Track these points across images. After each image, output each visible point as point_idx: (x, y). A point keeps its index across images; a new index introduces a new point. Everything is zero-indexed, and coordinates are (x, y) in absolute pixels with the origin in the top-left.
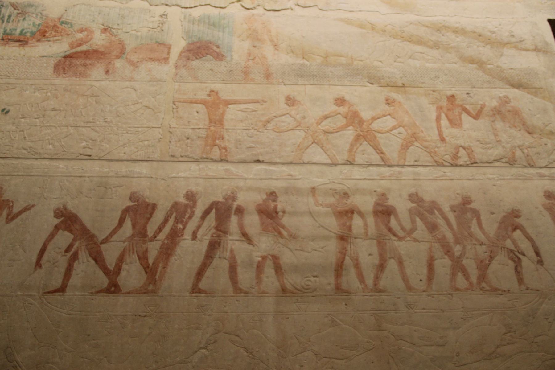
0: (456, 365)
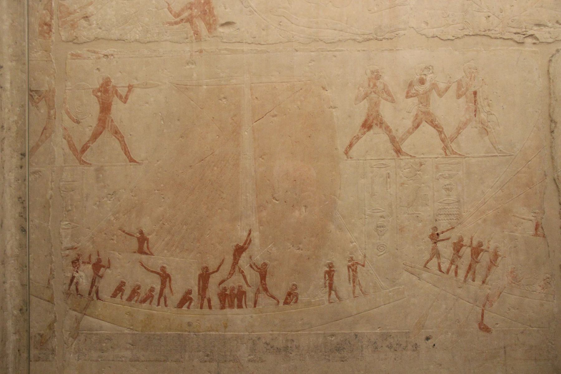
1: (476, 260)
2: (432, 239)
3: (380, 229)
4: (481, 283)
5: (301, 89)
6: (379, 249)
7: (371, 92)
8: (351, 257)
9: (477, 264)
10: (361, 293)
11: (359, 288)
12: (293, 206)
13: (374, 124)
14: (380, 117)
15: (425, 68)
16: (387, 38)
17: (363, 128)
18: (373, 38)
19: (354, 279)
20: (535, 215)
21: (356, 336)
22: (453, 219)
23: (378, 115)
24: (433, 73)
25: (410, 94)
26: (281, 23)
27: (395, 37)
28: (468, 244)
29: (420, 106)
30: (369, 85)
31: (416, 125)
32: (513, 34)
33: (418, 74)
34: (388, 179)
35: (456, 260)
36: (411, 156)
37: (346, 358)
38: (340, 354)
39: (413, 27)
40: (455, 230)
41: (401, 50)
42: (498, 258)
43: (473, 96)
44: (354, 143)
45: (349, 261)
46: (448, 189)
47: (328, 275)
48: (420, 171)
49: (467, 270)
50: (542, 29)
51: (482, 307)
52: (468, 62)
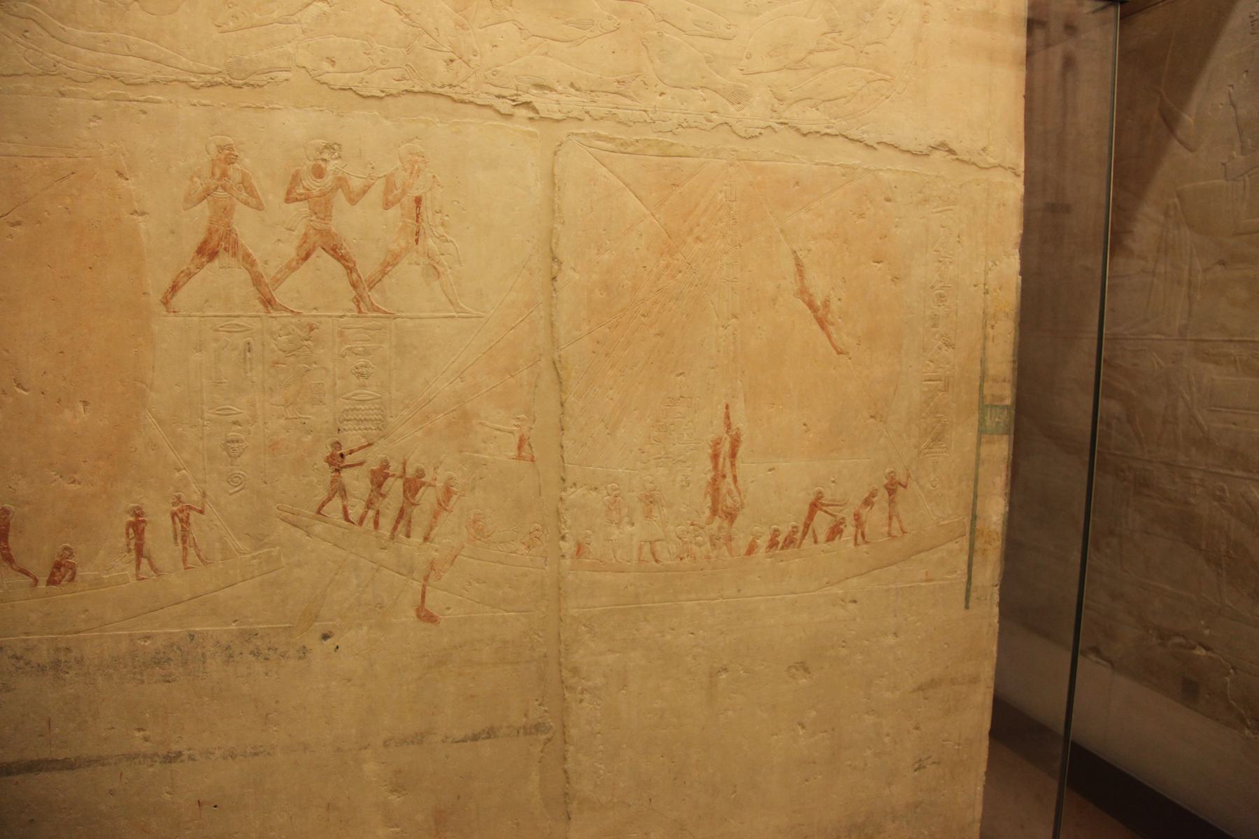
0: (743, 72)
1: (412, 501)
2: (331, 464)
3: (232, 445)
4: (421, 540)
5: (73, 173)
6: (232, 481)
7: (216, 188)
8: (177, 497)
9: (413, 507)
10: (200, 561)
11: (194, 552)
12: (59, 401)
13: (222, 250)
14: (234, 236)
15: (326, 147)
16: (251, 85)
17: (200, 256)
18: (223, 82)
19: (183, 536)
20: (519, 423)
21: (192, 637)
22: (370, 429)
23: (229, 232)
24: (340, 157)
25: (294, 195)
26: (27, 34)
27: (268, 83)
28: (398, 473)
29: (312, 219)
30: (213, 174)
31: (303, 254)
32: (494, 98)
33: (312, 159)
34: (248, 354)
35: (376, 500)
36: (292, 311)
37: (174, 677)
38: (163, 669)
39: (304, 67)
40: (374, 448)
41: (279, 109)
42: (451, 497)
43: (414, 205)
44: (180, 284)
45: (174, 504)
46: (362, 375)
47: (133, 529)
48: (309, 340)
49: (396, 518)
50: (547, 94)
51: (422, 581)
52: (408, 142)
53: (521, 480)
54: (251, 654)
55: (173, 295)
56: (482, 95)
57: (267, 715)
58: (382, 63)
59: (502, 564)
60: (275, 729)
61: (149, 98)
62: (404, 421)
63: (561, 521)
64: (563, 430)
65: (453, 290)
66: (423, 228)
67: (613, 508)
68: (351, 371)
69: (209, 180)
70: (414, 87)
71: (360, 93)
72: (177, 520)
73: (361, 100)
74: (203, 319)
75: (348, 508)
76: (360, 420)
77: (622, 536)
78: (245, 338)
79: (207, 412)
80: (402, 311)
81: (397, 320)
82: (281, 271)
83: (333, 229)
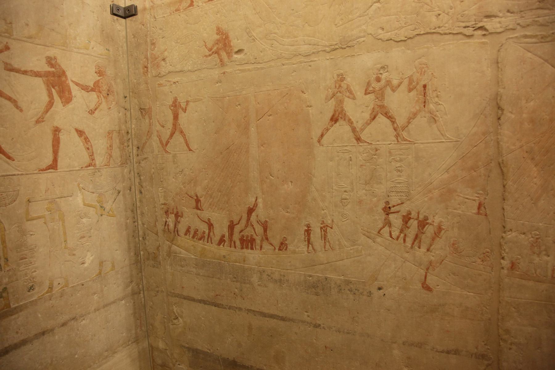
1: (422, 231)
2: (384, 211)
4: (425, 250)
5: (287, 94)
7: (337, 92)
13: (340, 118)
14: (345, 112)
15: (381, 68)
18: (338, 48)
19: (324, 237)
21: (326, 279)
22: (403, 196)
24: (387, 71)
25: (368, 91)
26: (273, 45)
27: (356, 44)
28: (415, 217)
29: (376, 101)
30: (336, 87)
34: (350, 162)
36: (368, 143)
40: (404, 205)
41: (361, 54)
42: (441, 231)
43: (423, 89)
45: (322, 224)
46: (399, 171)
51: (425, 270)
52: (419, 59)
53: (479, 225)
54: (348, 290)
55: (322, 139)
56: (456, 28)
57: (354, 317)
58: (405, 24)
59: (468, 267)
60: (356, 324)
61: (312, 60)
62: (419, 192)
63: (502, 249)
64: (504, 200)
65: (443, 129)
66: (428, 100)
67: (535, 245)
68: (394, 169)
69: (334, 90)
70: (421, 32)
71: (396, 40)
72: (322, 231)
73: (396, 43)
74: (333, 148)
75: (392, 232)
76: (398, 192)
77: (541, 261)
78: (349, 155)
79: (334, 187)
80: (418, 140)
81: (416, 144)
82: (363, 125)
83: (386, 104)
